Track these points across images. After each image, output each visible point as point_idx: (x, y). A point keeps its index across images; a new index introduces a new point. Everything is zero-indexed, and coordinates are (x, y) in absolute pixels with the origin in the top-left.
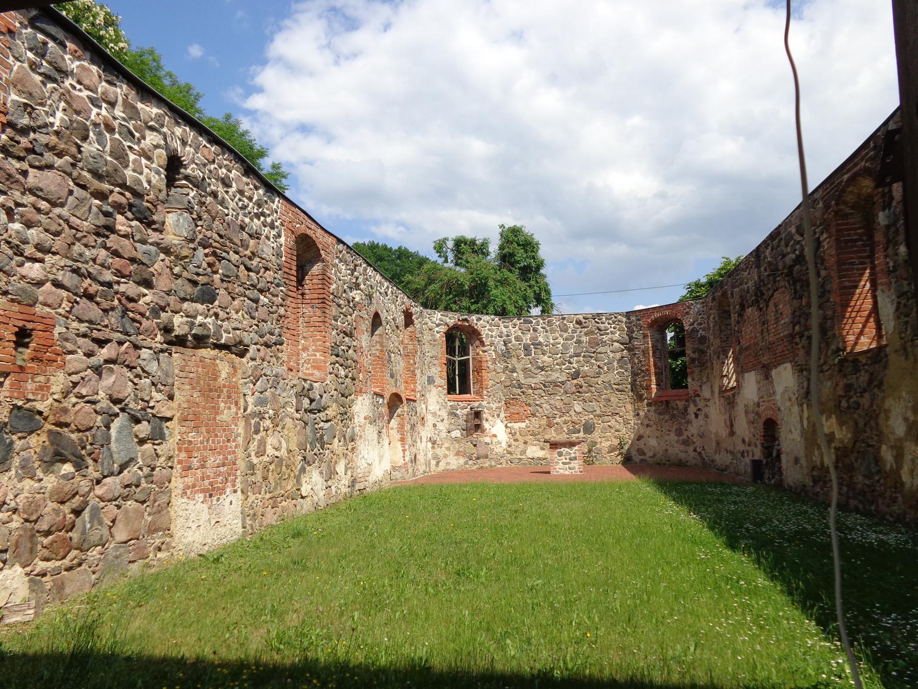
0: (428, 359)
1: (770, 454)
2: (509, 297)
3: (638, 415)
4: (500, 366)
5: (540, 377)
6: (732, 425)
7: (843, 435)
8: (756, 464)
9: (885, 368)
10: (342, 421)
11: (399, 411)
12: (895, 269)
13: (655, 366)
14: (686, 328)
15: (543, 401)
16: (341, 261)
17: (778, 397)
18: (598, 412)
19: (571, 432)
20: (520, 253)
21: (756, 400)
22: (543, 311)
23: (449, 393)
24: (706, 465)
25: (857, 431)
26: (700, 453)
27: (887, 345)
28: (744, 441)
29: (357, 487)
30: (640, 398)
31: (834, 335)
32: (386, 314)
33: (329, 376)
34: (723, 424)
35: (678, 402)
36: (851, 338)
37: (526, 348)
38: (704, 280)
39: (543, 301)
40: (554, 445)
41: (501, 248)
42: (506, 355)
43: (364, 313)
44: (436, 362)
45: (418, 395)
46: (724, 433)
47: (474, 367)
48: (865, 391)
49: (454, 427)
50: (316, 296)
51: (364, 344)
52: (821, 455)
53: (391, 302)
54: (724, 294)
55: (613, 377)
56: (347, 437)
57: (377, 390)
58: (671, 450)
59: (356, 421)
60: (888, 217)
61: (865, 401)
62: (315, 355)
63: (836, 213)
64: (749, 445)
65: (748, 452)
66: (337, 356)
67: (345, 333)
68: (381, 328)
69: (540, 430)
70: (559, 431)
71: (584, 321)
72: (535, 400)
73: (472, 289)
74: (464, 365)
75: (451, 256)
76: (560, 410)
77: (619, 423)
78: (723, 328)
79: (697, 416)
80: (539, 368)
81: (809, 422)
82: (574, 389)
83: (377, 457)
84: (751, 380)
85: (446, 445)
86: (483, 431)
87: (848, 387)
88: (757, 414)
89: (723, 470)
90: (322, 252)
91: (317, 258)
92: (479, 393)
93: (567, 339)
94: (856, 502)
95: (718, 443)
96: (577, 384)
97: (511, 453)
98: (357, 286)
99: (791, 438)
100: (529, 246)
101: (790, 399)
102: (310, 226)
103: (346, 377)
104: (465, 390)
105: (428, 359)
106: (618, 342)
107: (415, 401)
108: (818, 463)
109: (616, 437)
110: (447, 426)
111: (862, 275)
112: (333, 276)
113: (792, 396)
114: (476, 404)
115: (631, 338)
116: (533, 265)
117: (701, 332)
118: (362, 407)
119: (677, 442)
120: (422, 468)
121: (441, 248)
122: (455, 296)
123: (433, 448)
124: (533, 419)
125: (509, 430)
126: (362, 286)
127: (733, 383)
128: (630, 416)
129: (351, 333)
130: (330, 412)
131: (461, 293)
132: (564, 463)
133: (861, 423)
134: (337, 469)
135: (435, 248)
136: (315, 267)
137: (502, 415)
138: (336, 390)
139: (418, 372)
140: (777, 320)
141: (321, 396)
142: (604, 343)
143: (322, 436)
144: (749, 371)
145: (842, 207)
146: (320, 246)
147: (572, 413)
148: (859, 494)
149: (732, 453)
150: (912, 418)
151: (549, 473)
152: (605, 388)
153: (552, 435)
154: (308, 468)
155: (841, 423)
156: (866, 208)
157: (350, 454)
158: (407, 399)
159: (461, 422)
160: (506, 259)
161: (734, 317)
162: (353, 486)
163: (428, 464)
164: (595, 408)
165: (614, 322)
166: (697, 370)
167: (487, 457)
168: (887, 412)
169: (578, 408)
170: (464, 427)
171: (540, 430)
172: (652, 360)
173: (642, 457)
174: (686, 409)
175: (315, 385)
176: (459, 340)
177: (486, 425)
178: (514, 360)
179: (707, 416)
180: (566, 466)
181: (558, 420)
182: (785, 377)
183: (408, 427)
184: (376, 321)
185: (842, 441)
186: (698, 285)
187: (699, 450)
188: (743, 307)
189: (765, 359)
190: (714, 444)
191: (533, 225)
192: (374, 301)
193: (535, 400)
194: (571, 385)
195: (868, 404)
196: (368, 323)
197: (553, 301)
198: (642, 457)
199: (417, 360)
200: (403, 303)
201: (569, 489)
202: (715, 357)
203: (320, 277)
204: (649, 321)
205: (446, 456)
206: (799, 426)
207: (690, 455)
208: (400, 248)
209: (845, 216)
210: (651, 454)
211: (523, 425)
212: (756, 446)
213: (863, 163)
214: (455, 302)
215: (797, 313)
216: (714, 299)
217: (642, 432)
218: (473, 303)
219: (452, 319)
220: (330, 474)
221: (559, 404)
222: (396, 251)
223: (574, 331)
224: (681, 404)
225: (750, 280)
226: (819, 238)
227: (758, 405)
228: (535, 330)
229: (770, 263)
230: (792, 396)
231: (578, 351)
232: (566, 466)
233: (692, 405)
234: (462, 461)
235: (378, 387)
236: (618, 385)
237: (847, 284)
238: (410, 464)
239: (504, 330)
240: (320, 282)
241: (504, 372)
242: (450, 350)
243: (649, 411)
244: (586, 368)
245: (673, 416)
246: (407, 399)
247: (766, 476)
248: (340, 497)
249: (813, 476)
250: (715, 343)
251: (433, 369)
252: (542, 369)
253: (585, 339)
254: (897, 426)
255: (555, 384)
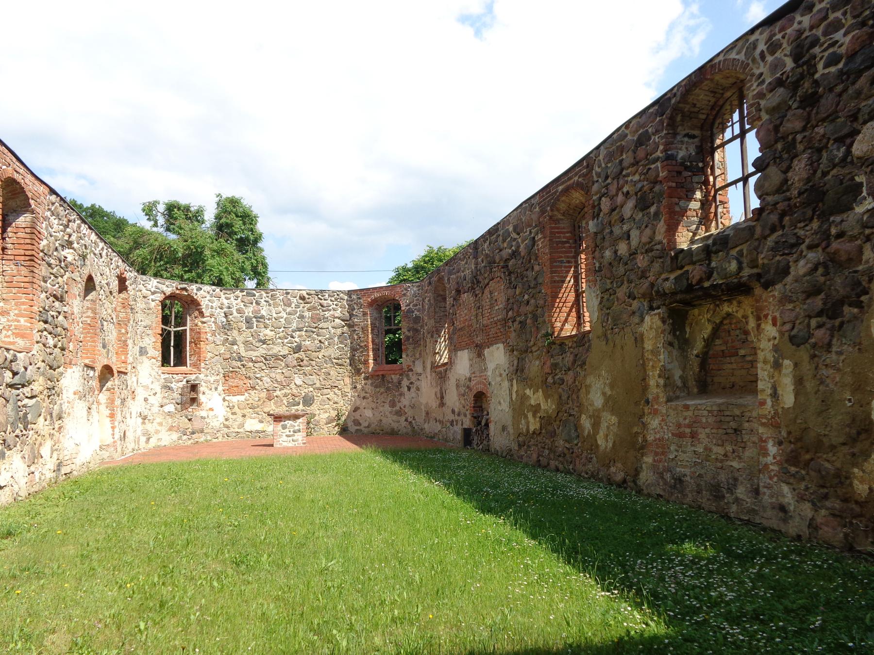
0: (141, 329)
1: (479, 423)
2: (226, 268)
3: (355, 387)
4: (219, 339)
5: (262, 350)
6: (442, 398)
7: (548, 406)
8: (467, 432)
9: (588, 350)
10: (49, 396)
11: (109, 384)
12: (600, 270)
13: (373, 342)
14: (403, 308)
15: (263, 375)
16: (53, 214)
17: (489, 373)
18: (318, 385)
19: (290, 405)
20: (238, 224)
21: (468, 375)
22: (258, 284)
23: (163, 366)
24: (415, 434)
25: (560, 403)
26: (411, 422)
27: (589, 332)
28: (453, 412)
29: (64, 470)
30: (358, 372)
31: (544, 322)
32: (100, 278)
33: (36, 346)
34: (434, 396)
35: (393, 376)
36: (558, 324)
37: (248, 321)
38: (410, 265)
39: (259, 274)
40: (278, 418)
41: (218, 217)
42: (227, 327)
43: (76, 275)
44: (149, 332)
45: (129, 367)
46: (434, 403)
47: (192, 338)
48: (569, 369)
49: (168, 401)
50: (22, 252)
51: (76, 310)
52: (528, 423)
53: (106, 266)
54: (441, 279)
55: (333, 352)
56: (54, 415)
57: (87, 361)
58: (384, 420)
59: (64, 396)
60: (597, 225)
61: (569, 378)
62: (19, 321)
63: (551, 217)
64: (459, 415)
65: (457, 421)
66: (46, 322)
67: (55, 296)
68: (94, 293)
69: (260, 403)
70: (278, 404)
71: (307, 296)
72: (255, 373)
73: (185, 257)
74: (180, 337)
75: (161, 221)
76: (280, 383)
77: (337, 395)
78: (437, 310)
79: (409, 389)
80: (260, 341)
81: (517, 395)
82: (295, 363)
83: (86, 435)
84: (464, 359)
85: (158, 420)
86: (199, 405)
87: (555, 366)
88: (468, 387)
89: (431, 437)
90: (32, 202)
91: (25, 207)
92: (196, 365)
93: (290, 314)
94: (557, 463)
95: (427, 413)
96: (299, 358)
97: (228, 427)
98: (69, 244)
99: (500, 409)
100: (248, 218)
101: (501, 375)
102: (18, 169)
103: (55, 346)
104: (180, 361)
105: (141, 329)
106: (339, 318)
107: (125, 374)
108: (524, 430)
109: (334, 409)
110: (160, 400)
111: (568, 272)
112: (43, 231)
113: (502, 372)
114: (193, 377)
115: (351, 315)
116: (252, 238)
117: (416, 312)
118: (72, 380)
119: (391, 412)
120: (130, 445)
121: (151, 210)
122: (167, 263)
123: (143, 423)
124: (252, 392)
125: (226, 403)
126: (75, 245)
127: (445, 359)
128: (348, 389)
129: (62, 297)
130: (37, 387)
131: (174, 260)
132: (288, 436)
133: (564, 397)
134: (42, 452)
135: (144, 210)
136: (22, 219)
137: (220, 388)
138: (43, 361)
139: (130, 342)
140: (492, 306)
141: (26, 369)
142: (326, 319)
143: (26, 415)
144: (462, 349)
145: (556, 213)
146: (30, 195)
147: (293, 386)
148: (559, 456)
149: (441, 422)
150: (609, 393)
151: (272, 445)
152: (326, 362)
153: (271, 407)
154: (8, 453)
155: (546, 397)
156: (576, 215)
157: (57, 434)
158: (118, 372)
159: (176, 395)
160: (222, 228)
161: (450, 301)
162: (59, 470)
163: (137, 441)
164: (315, 382)
165: (336, 299)
166: (411, 347)
167: (202, 431)
168: (588, 387)
169: (299, 381)
170: (179, 401)
171: (260, 403)
172: (370, 336)
173: (358, 428)
174: (400, 383)
175: (18, 355)
176: (177, 312)
177: (202, 398)
178: (235, 333)
179: (418, 389)
180: (289, 439)
181: (278, 393)
182: (497, 357)
183: (118, 402)
184: (90, 285)
185: (546, 411)
186: (405, 269)
187: (410, 419)
188: (458, 292)
189: (478, 340)
190: (424, 414)
191: (251, 200)
192: (88, 262)
193: (255, 373)
194: (292, 359)
195: (572, 380)
196: (81, 286)
197: (269, 275)
198: (358, 428)
199: (130, 329)
200: (118, 267)
201: (296, 463)
202: (429, 336)
203: (28, 230)
204: (369, 300)
205: (157, 432)
206: (508, 399)
207: (401, 425)
208: (93, 206)
209: (558, 221)
210: (366, 424)
211: (242, 398)
212: (465, 415)
213: (576, 178)
214: (166, 270)
215: (511, 301)
216: (430, 283)
217: (358, 403)
218: (186, 272)
219: (169, 287)
220: (34, 458)
221: (280, 378)
222: (87, 208)
223: (297, 306)
224: (395, 378)
225: (468, 269)
226: (534, 238)
227: (470, 380)
228: (258, 303)
229: (487, 256)
230: (502, 372)
231: (301, 326)
232: (289, 439)
233: (405, 379)
234: (175, 436)
235: (88, 358)
236: (338, 359)
237: (557, 279)
238: (119, 442)
239: (226, 302)
240: (28, 236)
241: (223, 345)
242: (165, 320)
243: (366, 384)
244: (307, 343)
245: (388, 389)
246: (118, 372)
247: (475, 442)
248: (44, 484)
249: (518, 441)
250: (430, 323)
251: (147, 339)
252: (264, 342)
253: (307, 314)
254: (596, 399)
255: (277, 357)
